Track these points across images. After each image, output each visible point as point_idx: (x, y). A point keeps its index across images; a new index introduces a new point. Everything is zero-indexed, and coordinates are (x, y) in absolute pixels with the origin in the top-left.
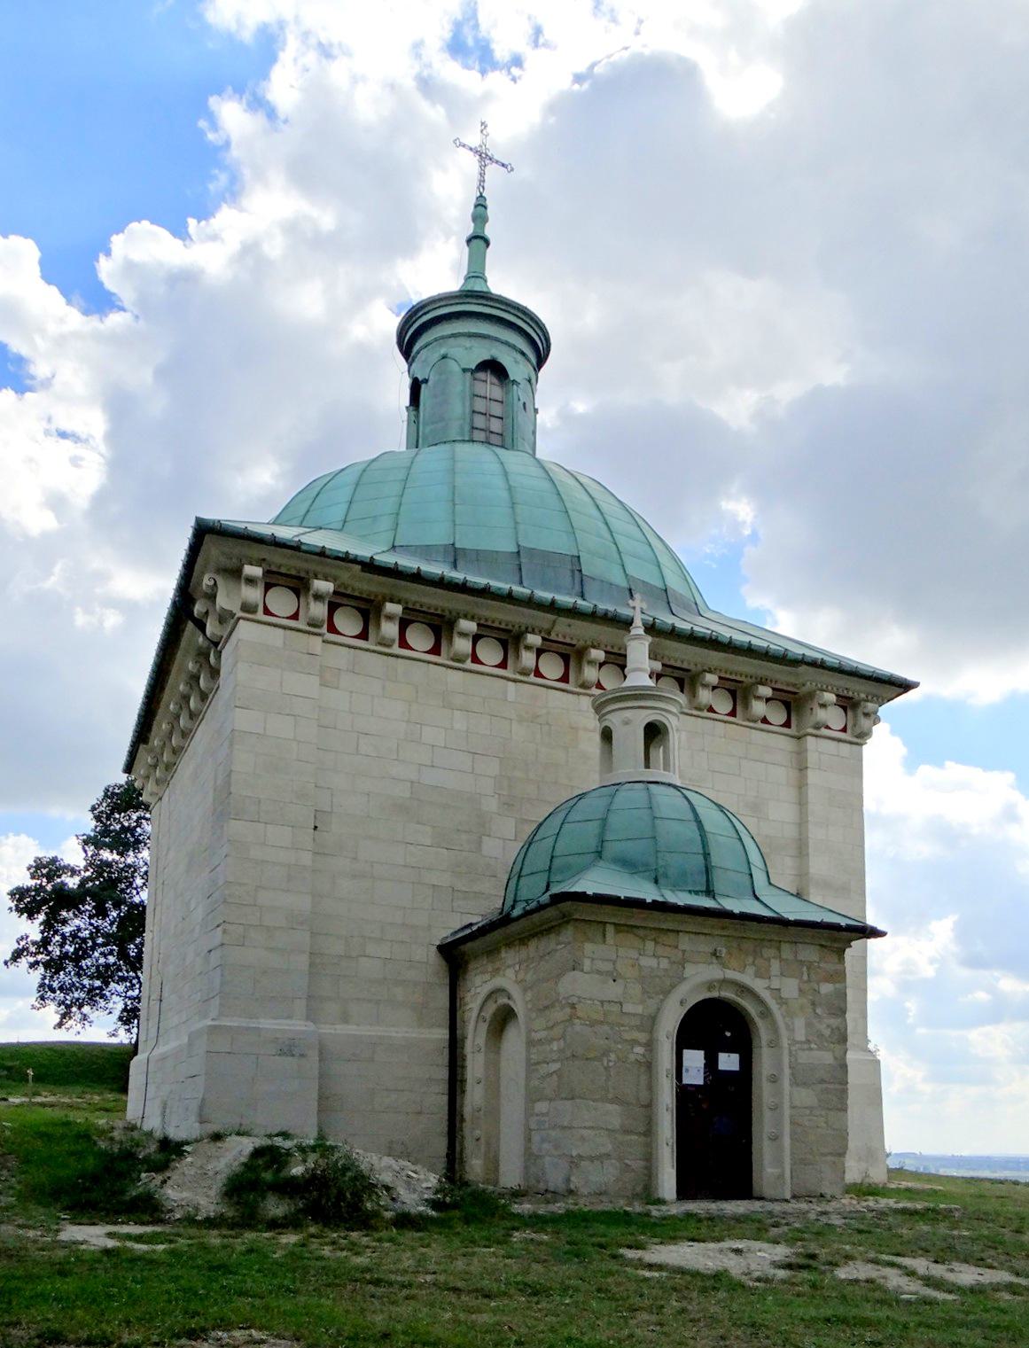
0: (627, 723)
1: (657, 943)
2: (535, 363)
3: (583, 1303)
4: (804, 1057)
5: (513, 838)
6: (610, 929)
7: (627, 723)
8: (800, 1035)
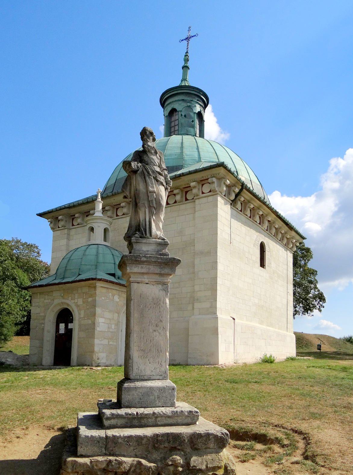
0: (99, 226)
1: (48, 296)
2: (204, 106)
3: (333, 457)
4: (83, 322)
5: (199, 272)
6: (38, 294)
7: (99, 226)
8: (82, 316)
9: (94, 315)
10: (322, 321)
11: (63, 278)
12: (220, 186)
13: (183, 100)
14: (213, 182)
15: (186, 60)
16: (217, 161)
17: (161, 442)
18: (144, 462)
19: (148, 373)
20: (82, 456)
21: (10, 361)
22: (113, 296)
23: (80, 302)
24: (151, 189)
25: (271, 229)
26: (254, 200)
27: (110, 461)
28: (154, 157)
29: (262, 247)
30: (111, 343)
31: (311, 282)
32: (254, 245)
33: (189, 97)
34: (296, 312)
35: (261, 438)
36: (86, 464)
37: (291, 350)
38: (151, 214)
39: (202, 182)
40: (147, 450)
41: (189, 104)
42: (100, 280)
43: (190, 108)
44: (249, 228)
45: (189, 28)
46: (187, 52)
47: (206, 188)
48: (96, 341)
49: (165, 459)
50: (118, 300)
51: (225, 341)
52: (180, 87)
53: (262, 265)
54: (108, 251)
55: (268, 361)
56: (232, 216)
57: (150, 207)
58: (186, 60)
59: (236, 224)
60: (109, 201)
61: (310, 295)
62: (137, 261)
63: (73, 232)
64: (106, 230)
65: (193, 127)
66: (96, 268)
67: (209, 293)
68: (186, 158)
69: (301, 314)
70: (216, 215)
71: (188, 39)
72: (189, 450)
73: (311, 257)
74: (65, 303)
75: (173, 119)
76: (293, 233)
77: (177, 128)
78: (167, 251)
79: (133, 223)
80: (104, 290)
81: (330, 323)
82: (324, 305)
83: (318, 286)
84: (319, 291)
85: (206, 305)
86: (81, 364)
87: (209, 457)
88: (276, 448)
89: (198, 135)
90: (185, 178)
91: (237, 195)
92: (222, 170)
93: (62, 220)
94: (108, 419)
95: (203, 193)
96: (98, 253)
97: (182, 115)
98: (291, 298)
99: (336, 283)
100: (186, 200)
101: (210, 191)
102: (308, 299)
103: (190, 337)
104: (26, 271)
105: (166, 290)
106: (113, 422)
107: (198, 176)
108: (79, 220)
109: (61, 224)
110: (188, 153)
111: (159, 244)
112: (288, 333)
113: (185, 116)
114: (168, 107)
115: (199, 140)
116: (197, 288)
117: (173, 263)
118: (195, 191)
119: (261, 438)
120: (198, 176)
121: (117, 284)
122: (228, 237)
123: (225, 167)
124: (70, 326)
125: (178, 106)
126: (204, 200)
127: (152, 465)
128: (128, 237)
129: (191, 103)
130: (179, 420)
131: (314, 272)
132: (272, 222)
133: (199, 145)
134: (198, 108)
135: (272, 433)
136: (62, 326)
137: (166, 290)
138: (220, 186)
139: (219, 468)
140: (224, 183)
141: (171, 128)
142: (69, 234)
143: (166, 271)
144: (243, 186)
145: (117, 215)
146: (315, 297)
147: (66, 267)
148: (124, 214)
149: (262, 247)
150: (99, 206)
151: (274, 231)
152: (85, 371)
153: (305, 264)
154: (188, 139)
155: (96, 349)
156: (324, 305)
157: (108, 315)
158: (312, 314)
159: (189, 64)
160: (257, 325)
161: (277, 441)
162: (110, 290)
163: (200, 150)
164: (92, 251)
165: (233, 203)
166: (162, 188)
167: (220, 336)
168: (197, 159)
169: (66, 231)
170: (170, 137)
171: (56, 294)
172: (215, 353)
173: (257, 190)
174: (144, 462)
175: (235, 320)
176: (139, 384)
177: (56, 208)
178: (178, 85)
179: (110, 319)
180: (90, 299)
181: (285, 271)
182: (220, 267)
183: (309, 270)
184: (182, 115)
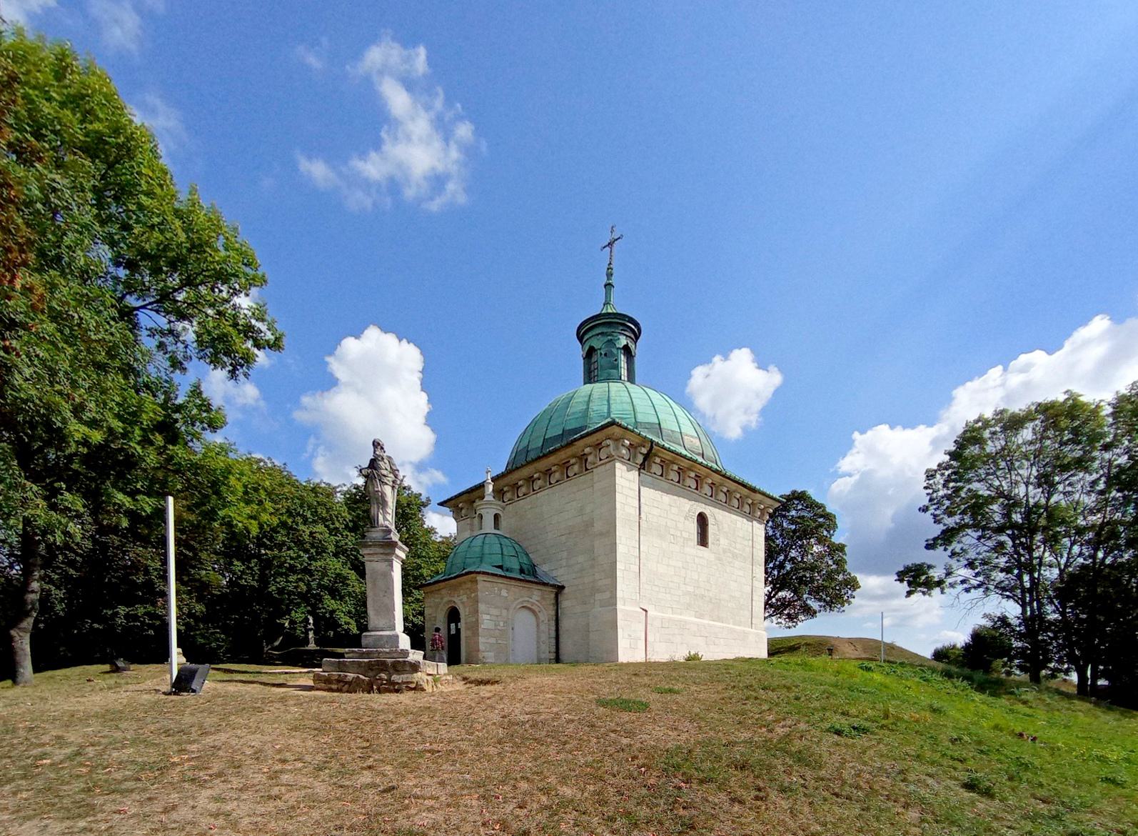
12: (617, 448)
13: (602, 334)
14: (608, 446)
15: (609, 275)
17: (373, 665)
18: (361, 676)
22: (500, 590)
23: (465, 598)
26: (678, 459)
29: (702, 520)
32: (686, 518)
37: (763, 653)
39: (598, 446)
41: (609, 338)
43: (611, 343)
44: (675, 497)
48: (481, 640)
50: (506, 595)
53: (703, 540)
57: (377, 503)
58: (609, 275)
64: (496, 517)
65: (616, 367)
67: (608, 581)
68: (592, 414)
71: (610, 244)
72: (391, 671)
74: (451, 601)
75: (593, 360)
76: (759, 497)
80: (488, 584)
82: (854, 594)
86: (469, 662)
87: (405, 676)
90: (581, 443)
92: (615, 429)
95: (601, 460)
97: (601, 354)
100: (587, 469)
110: (595, 408)
112: (753, 630)
113: (606, 355)
125: (596, 343)
127: (367, 678)
129: (612, 336)
132: (717, 484)
134: (623, 341)
136: (453, 626)
139: (412, 683)
140: (623, 445)
149: (702, 520)
150: (490, 488)
154: (615, 387)
155: (481, 647)
156: (854, 594)
157: (494, 612)
158: (842, 609)
159: (613, 281)
162: (495, 584)
163: (611, 402)
164: (478, 541)
167: (620, 631)
168: (606, 414)
171: (443, 592)
172: (614, 650)
174: (361, 676)
175: (649, 613)
176: (373, 633)
178: (598, 313)
180: (473, 595)
184: (601, 354)
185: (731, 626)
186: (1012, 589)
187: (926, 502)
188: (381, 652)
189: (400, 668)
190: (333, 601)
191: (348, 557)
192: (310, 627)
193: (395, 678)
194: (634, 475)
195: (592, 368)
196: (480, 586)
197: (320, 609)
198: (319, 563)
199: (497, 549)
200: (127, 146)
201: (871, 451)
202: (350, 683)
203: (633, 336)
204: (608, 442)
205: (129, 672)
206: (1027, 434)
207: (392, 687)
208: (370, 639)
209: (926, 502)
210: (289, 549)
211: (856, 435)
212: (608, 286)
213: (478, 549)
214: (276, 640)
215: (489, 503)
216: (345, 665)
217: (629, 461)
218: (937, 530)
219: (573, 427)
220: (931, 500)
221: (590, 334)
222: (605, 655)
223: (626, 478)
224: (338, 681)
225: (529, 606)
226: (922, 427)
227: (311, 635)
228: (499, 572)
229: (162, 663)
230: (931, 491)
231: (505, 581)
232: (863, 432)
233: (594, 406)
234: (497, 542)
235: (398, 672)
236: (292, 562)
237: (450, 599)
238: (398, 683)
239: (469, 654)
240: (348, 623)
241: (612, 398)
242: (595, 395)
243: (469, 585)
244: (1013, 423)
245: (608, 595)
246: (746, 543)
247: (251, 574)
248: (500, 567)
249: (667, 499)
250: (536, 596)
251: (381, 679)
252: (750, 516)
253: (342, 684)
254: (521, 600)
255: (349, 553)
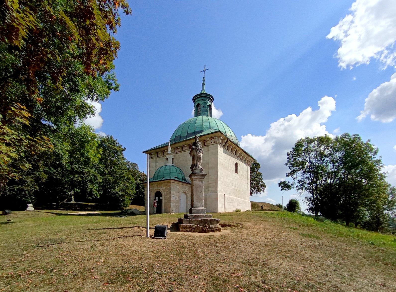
8: (165, 194)
9: (170, 193)
10: (268, 198)
11: (157, 179)
12: (218, 140)
13: (203, 100)
15: (204, 81)
16: (218, 129)
18: (199, 226)
19: (198, 205)
20: (184, 224)
21: (137, 212)
24: (198, 154)
25: (240, 156)
27: (191, 225)
28: (199, 144)
30: (177, 204)
31: (260, 179)
33: (205, 98)
34: (251, 194)
35: (230, 226)
36: (185, 225)
37: (249, 208)
38: (198, 161)
39: (211, 138)
40: (199, 223)
42: (172, 180)
43: (205, 103)
44: (231, 157)
45: (205, 66)
46: (204, 77)
47: (213, 141)
48: (171, 204)
49: (204, 225)
51: (221, 203)
52: (201, 94)
53: (236, 172)
54: (174, 168)
55: (238, 211)
56: (224, 152)
57: (198, 159)
58: (204, 81)
59: (225, 155)
60: (172, 146)
61: (259, 185)
62: (195, 175)
63: (158, 159)
64: (173, 159)
65: (207, 111)
66: (170, 175)
67: (214, 184)
69: (255, 193)
70: (217, 152)
71: (204, 71)
72: (210, 223)
73: (260, 167)
75: (199, 108)
76: (250, 158)
77: (200, 112)
78: (203, 172)
79: (193, 163)
80: (173, 184)
81: (271, 199)
83: (263, 181)
84: (263, 183)
85: (214, 189)
86: (166, 212)
87: (215, 225)
88: (233, 227)
89: (209, 115)
91: (226, 143)
92: (219, 133)
93: (153, 154)
94: (189, 216)
95: (212, 143)
96: (170, 169)
98: (249, 186)
99: (274, 180)
100: (205, 145)
101: (215, 142)
102: (258, 187)
103: (207, 202)
104: (133, 176)
105: (203, 183)
106: (190, 217)
107: (210, 136)
108: (160, 154)
109: (153, 156)
110: (205, 125)
111: (200, 170)
112: (247, 201)
113: (203, 107)
114: (196, 103)
115: (209, 117)
116: (210, 182)
117: (204, 175)
118: (208, 142)
119: (230, 226)
120: (210, 136)
121: (177, 181)
122: (222, 161)
123: (221, 132)
124: (161, 198)
125: (201, 103)
126: (212, 146)
128: (192, 168)
130: (207, 217)
131: (261, 174)
133: (210, 121)
134: (209, 103)
135: (232, 224)
137: (203, 183)
138: (218, 140)
139: (217, 228)
141: (197, 112)
142: (156, 160)
143: (203, 177)
144: (228, 139)
145: (176, 152)
146: (261, 186)
147: (158, 175)
148: (179, 152)
151: (241, 157)
152: (168, 215)
153: (257, 170)
154: (205, 117)
156: (265, 189)
157: (175, 194)
158: (260, 193)
159: (205, 83)
160: (234, 197)
161: (234, 226)
163: (210, 123)
164: (168, 168)
165: (224, 146)
166: (201, 153)
167: (219, 201)
169: (155, 159)
170: (197, 117)
171: (154, 185)
173: (234, 140)
174: (199, 226)
175: (225, 195)
177: (150, 149)
179: (176, 195)
181: (246, 175)
182: (219, 174)
183: (259, 173)
185: (243, 200)
186: (309, 189)
187: (287, 162)
188: (202, 216)
189: (212, 222)
190: (91, 185)
191: (96, 168)
192: (72, 194)
193: (211, 226)
194: (222, 149)
195: (198, 111)
196: (172, 184)
197: (86, 188)
198: (86, 170)
199: (175, 171)
200: (107, 14)
201: (247, 142)
202: (194, 228)
203: (211, 101)
204: (216, 137)
205: (11, 215)
206: (312, 145)
207: (210, 230)
208: (195, 210)
209: (287, 162)
210: (75, 164)
211: (242, 136)
212: (203, 84)
213: (168, 171)
214: (64, 200)
215: (170, 154)
216: (192, 221)
217: (221, 144)
218: (289, 171)
219: (198, 130)
220: (288, 162)
221: (200, 99)
222: (213, 210)
223: (220, 149)
224: (190, 227)
225: (185, 192)
226: (260, 136)
227: (73, 197)
228: (176, 179)
229: (24, 210)
230: (288, 159)
231: (179, 183)
232: (244, 136)
233: (205, 124)
234: (175, 168)
235: (211, 223)
236: (77, 169)
237: (157, 188)
238: (213, 228)
239: (165, 210)
240: (96, 194)
241: (210, 122)
242: (204, 120)
243: (166, 184)
244: (310, 141)
245: (214, 189)
246: (246, 172)
247: (58, 173)
248: (177, 177)
249: (229, 157)
250: (187, 188)
251: (206, 227)
252: (247, 164)
253: (191, 229)
254: (183, 189)
255: (97, 167)
